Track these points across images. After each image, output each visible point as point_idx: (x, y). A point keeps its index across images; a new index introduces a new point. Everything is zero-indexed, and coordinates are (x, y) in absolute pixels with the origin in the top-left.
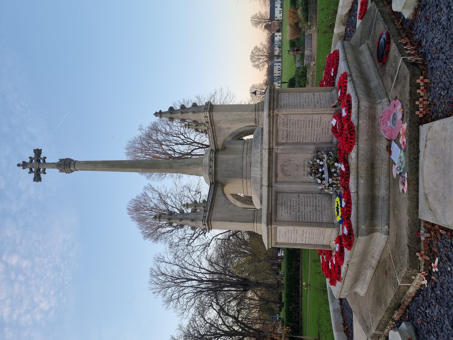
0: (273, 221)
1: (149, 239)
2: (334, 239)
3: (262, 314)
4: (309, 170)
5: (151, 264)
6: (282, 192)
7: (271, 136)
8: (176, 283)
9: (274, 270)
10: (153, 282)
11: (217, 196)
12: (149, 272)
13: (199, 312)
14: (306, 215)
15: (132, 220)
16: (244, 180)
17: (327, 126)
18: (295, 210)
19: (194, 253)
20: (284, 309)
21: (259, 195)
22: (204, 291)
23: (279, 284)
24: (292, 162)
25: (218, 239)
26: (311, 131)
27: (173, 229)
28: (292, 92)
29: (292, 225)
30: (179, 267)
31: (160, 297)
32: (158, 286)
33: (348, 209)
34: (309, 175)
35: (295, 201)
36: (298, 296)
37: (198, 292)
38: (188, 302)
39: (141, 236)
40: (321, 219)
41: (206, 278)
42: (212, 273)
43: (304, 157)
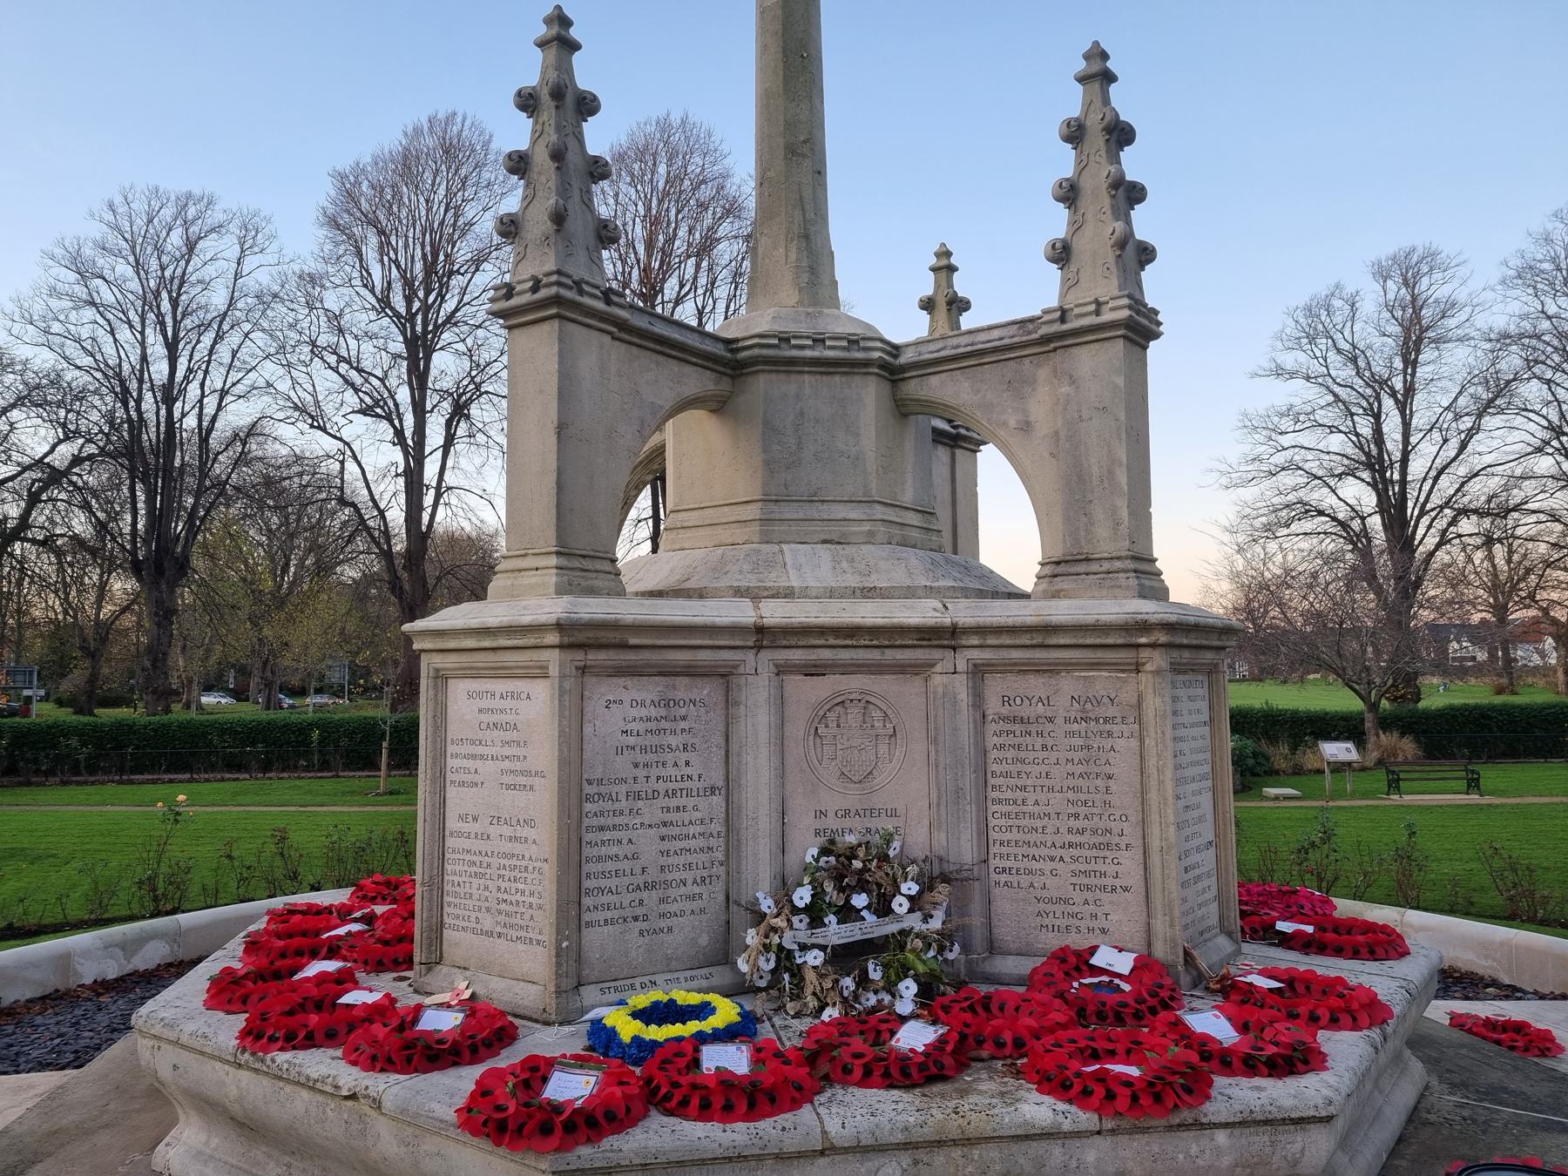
0: (579, 656)
1: (333, 193)
2: (481, 992)
3: (41, 635)
4: (851, 839)
5: (231, 199)
6: (729, 702)
7: (1025, 640)
8: (157, 294)
9: (220, 676)
10: (156, 204)
11: (675, 367)
12: (197, 192)
13: (38, 387)
14: (616, 835)
15: (410, 130)
16: (753, 511)
17: (1083, 924)
18: (641, 773)
19: (282, 371)
20: (65, 715)
21: (688, 585)
22: (125, 404)
23: (166, 695)
24: (883, 749)
25: (342, 462)
26: (1049, 839)
27: (378, 290)
28: (1213, 736)
29: (563, 762)
30: (223, 308)
31: (97, 231)
32: (140, 222)
33: (718, 1102)
34: (821, 840)
35: (689, 771)
36: (121, 771)
37: (122, 382)
38: (78, 341)
39: (345, 164)
40: (600, 916)
41: (183, 415)
42: (204, 440)
43: (907, 804)
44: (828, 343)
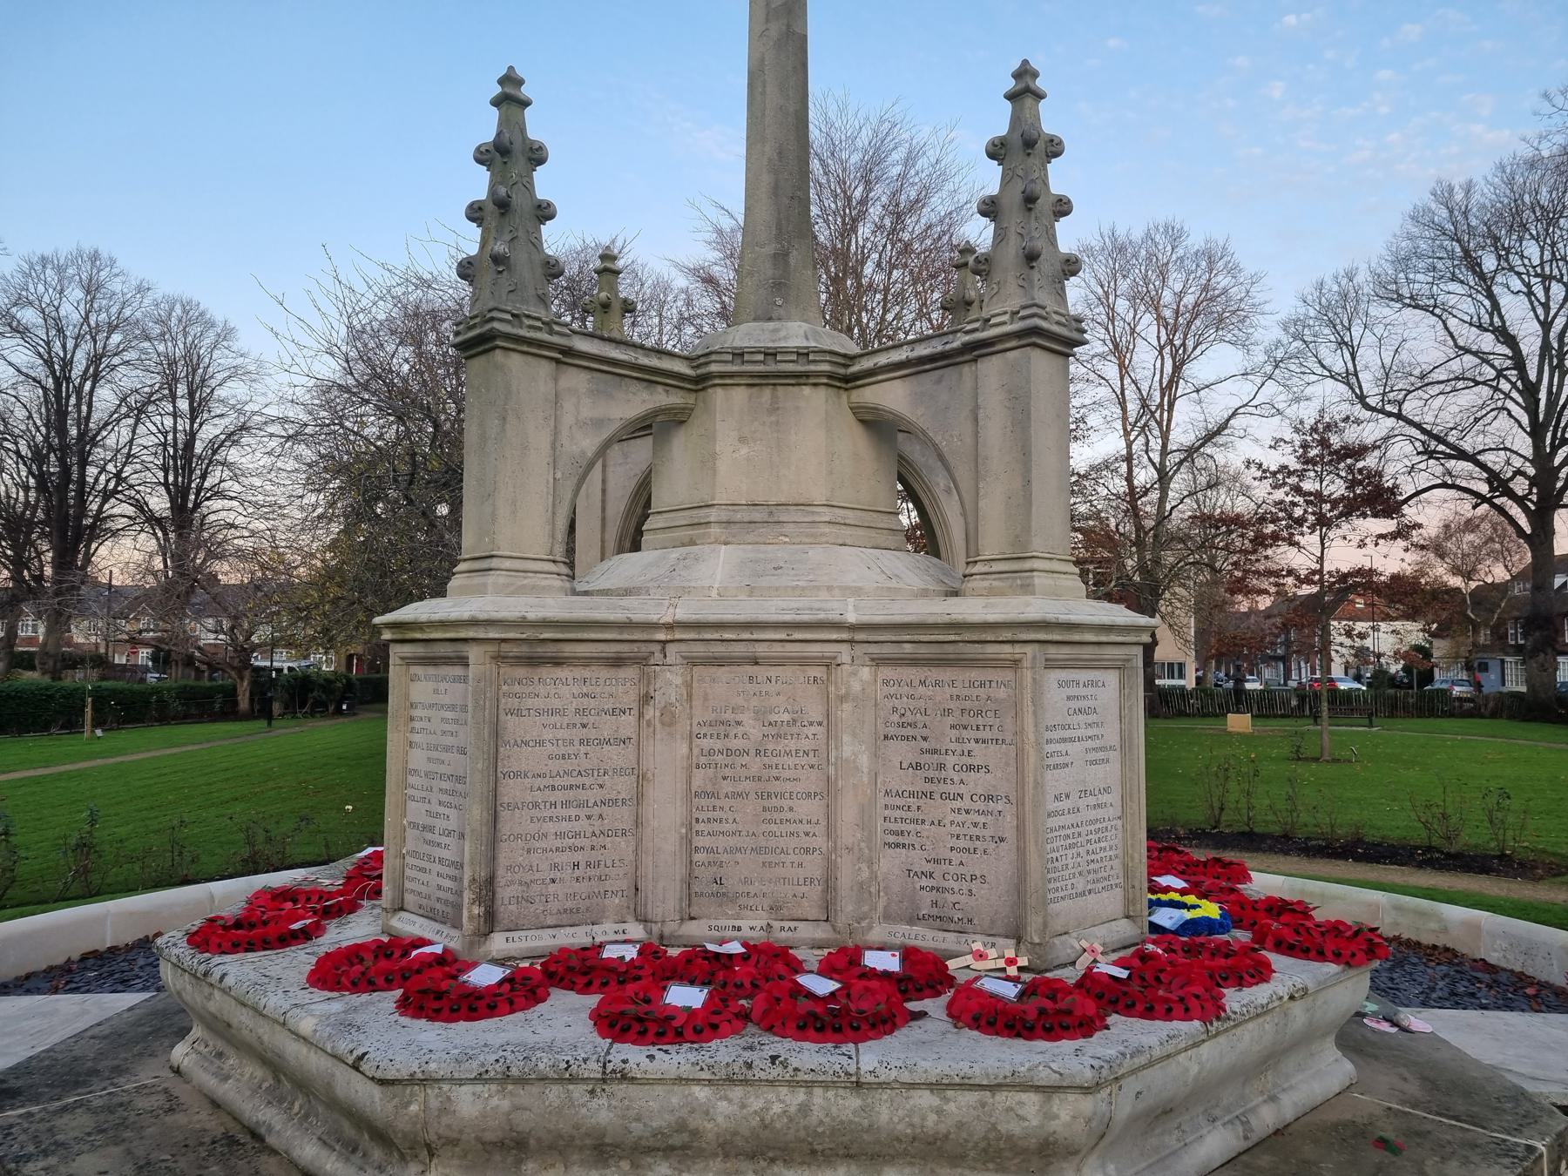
44: (746, 357)
